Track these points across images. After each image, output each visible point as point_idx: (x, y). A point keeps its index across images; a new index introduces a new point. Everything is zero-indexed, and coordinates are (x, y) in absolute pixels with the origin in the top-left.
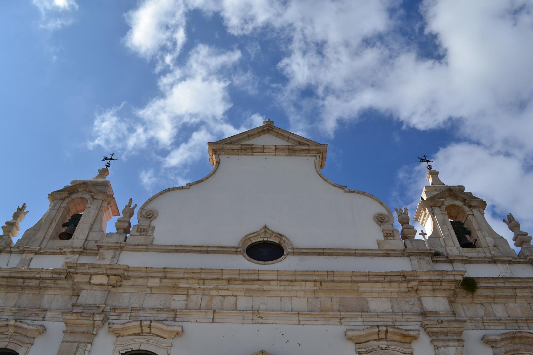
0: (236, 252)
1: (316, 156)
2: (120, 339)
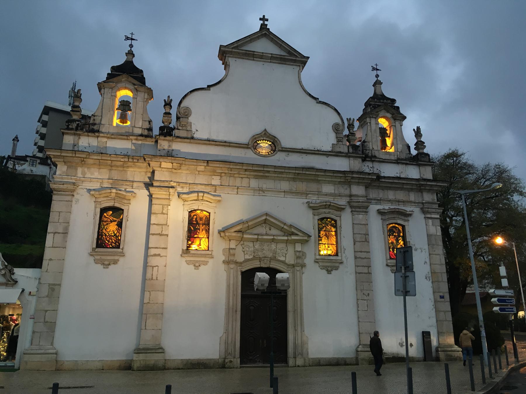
0: (248, 148)
1: (299, 66)
2: (186, 203)
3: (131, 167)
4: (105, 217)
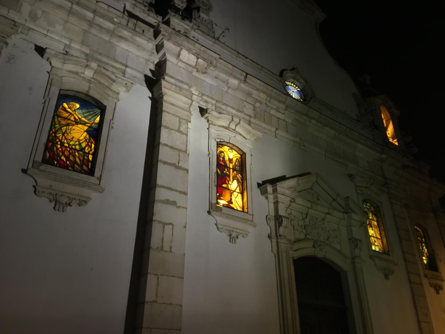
3: (126, 40)
4: (65, 109)
